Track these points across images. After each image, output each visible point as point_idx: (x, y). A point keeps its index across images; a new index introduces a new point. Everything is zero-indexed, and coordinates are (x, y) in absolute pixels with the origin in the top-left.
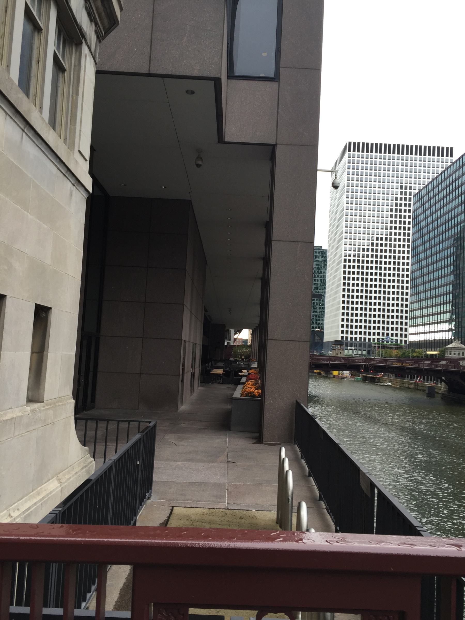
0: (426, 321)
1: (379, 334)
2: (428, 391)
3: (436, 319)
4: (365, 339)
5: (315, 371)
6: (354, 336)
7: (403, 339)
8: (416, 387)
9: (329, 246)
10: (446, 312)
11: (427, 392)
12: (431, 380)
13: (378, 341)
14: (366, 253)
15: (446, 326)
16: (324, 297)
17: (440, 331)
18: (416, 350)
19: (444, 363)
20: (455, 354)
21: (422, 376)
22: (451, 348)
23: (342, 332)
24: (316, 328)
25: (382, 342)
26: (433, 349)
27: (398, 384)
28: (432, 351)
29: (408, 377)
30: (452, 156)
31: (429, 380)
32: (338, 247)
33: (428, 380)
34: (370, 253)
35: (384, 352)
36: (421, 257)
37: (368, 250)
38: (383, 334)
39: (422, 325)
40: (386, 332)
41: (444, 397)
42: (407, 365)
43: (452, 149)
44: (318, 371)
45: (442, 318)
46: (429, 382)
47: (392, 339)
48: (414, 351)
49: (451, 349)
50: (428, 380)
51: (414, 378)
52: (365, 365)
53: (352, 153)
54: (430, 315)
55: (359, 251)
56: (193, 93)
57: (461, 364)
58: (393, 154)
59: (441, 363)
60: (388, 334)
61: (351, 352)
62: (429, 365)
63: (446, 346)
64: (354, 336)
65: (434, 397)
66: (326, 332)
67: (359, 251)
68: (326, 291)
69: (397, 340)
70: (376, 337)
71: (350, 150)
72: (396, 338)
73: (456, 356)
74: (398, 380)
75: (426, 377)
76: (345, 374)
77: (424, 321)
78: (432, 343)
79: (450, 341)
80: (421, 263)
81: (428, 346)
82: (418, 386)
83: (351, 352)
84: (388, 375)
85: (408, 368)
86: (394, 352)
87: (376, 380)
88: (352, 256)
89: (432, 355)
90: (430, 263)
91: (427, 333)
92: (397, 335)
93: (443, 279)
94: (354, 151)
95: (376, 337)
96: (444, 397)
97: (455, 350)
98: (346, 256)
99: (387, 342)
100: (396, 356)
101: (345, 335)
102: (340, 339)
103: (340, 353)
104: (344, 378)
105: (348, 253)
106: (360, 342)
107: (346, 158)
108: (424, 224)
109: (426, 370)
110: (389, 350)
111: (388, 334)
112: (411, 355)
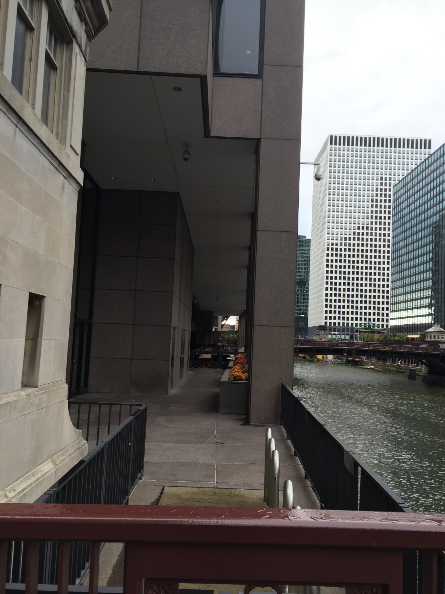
5: (300, 355)
7: (385, 323)
8: (398, 369)
9: (312, 236)
12: (412, 363)
13: (360, 326)
15: (426, 311)
16: (308, 284)
18: (397, 334)
19: (424, 346)
20: (434, 338)
21: (403, 360)
22: (431, 332)
23: (326, 318)
24: (300, 314)
26: (414, 333)
27: (380, 367)
28: (412, 335)
29: (390, 360)
30: (430, 148)
31: (410, 362)
33: (409, 362)
35: (366, 336)
41: (425, 379)
42: (389, 348)
43: (430, 141)
44: (303, 355)
46: (410, 364)
48: (395, 335)
50: (409, 362)
51: (396, 361)
52: (348, 349)
53: (333, 146)
54: (410, 301)
57: (441, 347)
59: (422, 346)
61: (334, 337)
62: (410, 348)
66: (310, 317)
68: (310, 278)
69: (379, 325)
71: (331, 144)
72: (378, 323)
73: (436, 339)
74: (380, 363)
75: (407, 360)
79: (430, 325)
81: (409, 330)
82: (399, 368)
83: (334, 337)
84: (371, 358)
85: (390, 352)
86: (376, 337)
87: (359, 364)
89: (413, 339)
96: (425, 379)
99: (370, 327)
100: (378, 340)
101: (328, 321)
102: (324, 325)
103: (324, 337)
104: (328, 362)
105: (331, 241)
106: (343, 327)
109: (407, 353)
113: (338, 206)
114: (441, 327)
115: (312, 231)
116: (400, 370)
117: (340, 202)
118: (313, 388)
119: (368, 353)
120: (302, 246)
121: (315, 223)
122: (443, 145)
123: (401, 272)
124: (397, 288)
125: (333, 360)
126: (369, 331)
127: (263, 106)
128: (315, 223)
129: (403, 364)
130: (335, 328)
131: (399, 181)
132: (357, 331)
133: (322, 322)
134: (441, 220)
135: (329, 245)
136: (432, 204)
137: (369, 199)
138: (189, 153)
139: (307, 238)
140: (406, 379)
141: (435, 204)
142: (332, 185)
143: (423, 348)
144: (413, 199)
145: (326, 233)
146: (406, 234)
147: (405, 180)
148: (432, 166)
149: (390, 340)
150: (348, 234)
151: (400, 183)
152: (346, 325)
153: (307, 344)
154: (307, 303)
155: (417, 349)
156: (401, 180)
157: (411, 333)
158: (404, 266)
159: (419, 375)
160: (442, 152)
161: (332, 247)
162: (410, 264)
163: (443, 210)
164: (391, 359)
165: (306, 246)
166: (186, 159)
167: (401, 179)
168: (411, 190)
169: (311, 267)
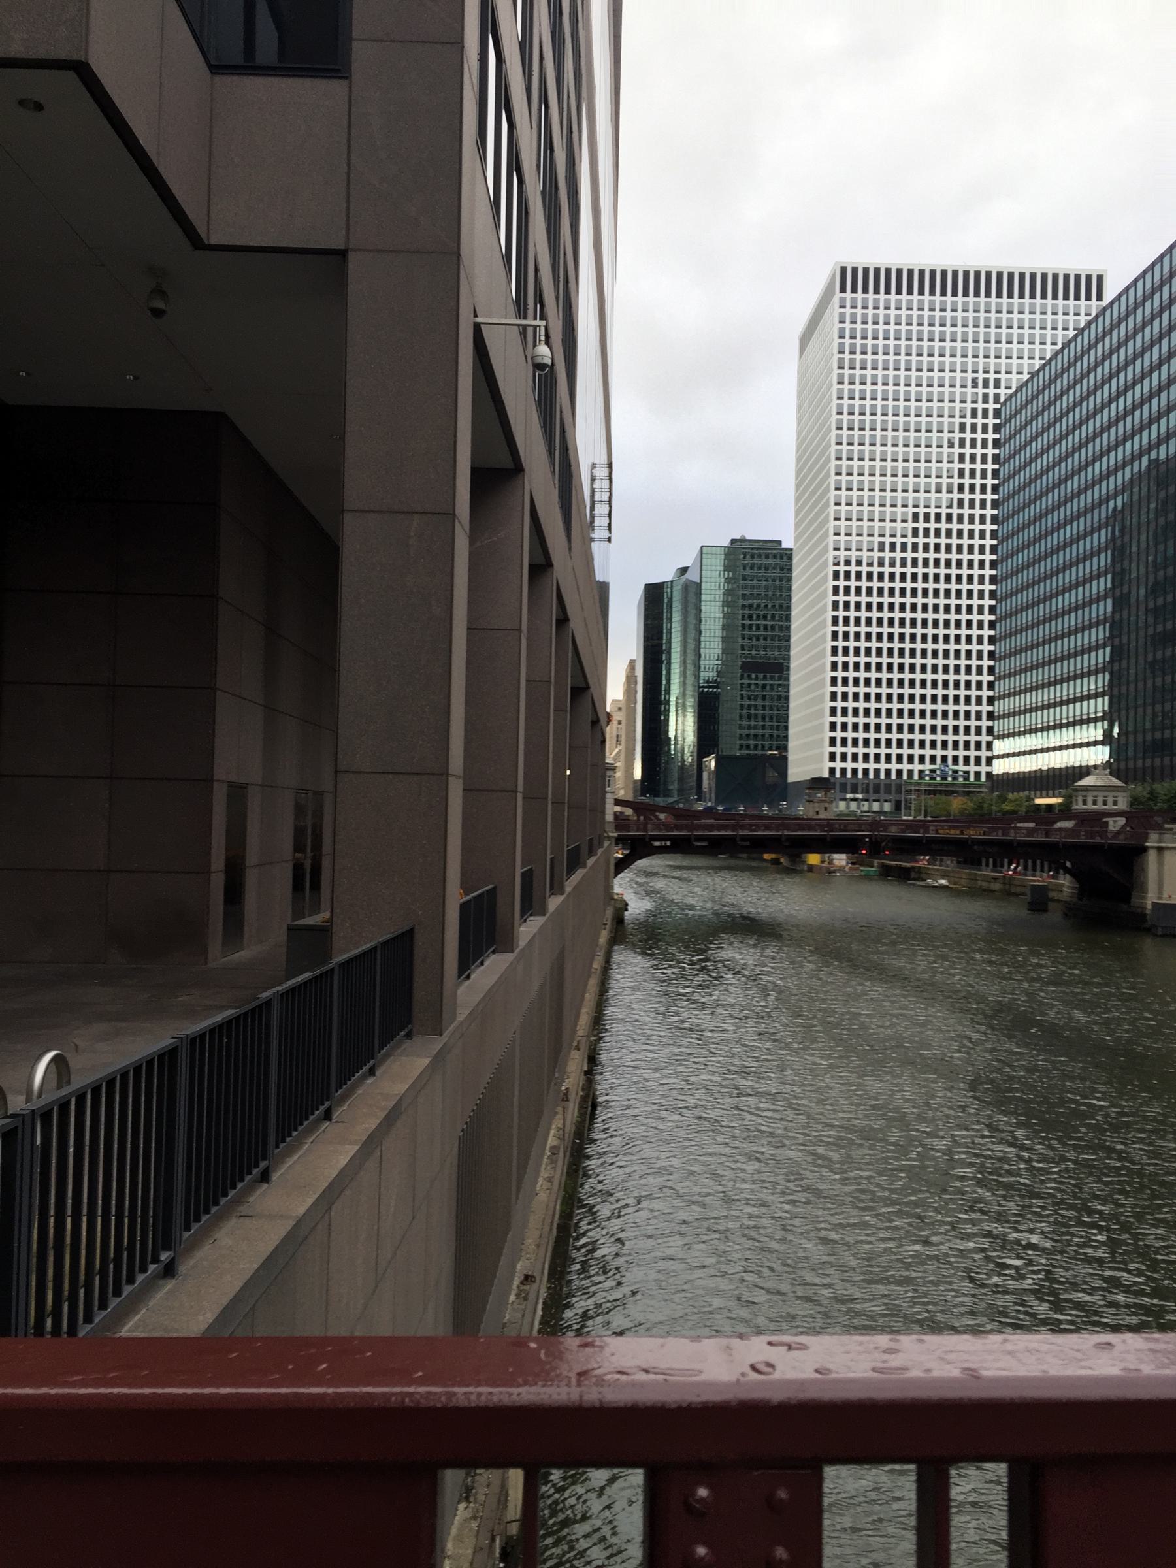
1: (922, 759)
5: (767, 856)
7: (984, 769)
8: (1007, 887)
9: (797, 539)
11: (1029, 898)
12: (1042, 871)
13: (921, 778)
14: (898, 555)
15: (1096, 732)
16: (788, 668)
18: (1010, 796)
19: (1068, 824)
20: (1095, 803)
21: (1021, 861)
22: (1087, 789)
23: (832, 757)
27: (963, 882)
28: (1048, 796)
29: (987, 865)
31: (1038, 867)
33: (1034, 869)
34: (909, 555)
35: (931, 803)
37: (904, 547)
40: (939, 752)
41: (1070, 911)
43: (1100, 279)
44: (773, 856)
46: (1038, 873)
47: (956, 772)
48: (1003, 799)
49: (1087, 790)
50: (1034, 869)
51: (1002, 866)
53: (848, 295)
55: (881, 549)
56: (39, 107)
57: (1111, 828)
59: (1059, 825)
62: (1030, 831)
64: (861, 766)
65: (1046, 911)
66: (792, 756)
67: (881, 549)
69: (967, 773)
71: (843, 290)
72: (966, 768)
73: (1100, 807)
74: (966, 871)
75: (1038, 862)
76: (837, 863)
80: (1061, 575)
84: (941, 861)
87: (913, 875)
89: (1049, 806)
92: (967, 760)
95: (916, 767)
96: (1070, 911)
97: (1095, 793)
99: (944, 778)
101: (838, 765)
102: (826, 775)
103: (826, 809)
104: (834, 871)
105: (843, 554)
106: (877, 781)
107: (834, 310)
110: (944, 798)
112: (994, 808)
113: (861, 459)
114: (1111, 774)
115: (797, 526)
116: (1013, 890)
117: (867, 448)
119: (937, 848)
122: (1171, 248)
123: (1038, 625)
124: (1032, 668)
125: (847, 869)
126: (940, 789)
129: (1020, 874)
130: (890, 785)
131: (1033, 375)
132: (909, 792)
133: (821, 770)
134: (1136, 483)
136: (1121, 432)
139: (784, 546)
140: (1024, 913)
141: (1121, 438)
142: (846, 402)
143: (1061, 829)
144: (1058, 432)
145: (832, 532)
146: (1032, 532)
147: (1093, 326)
150: (887, 534)
151: (1035, 379)
152: (882, 776)
153: (767, 828)
154: (786, 719)
155: (1047, 835)
156: (1039, 371)
157: (1044, 793)
158: (1027, 617)
160: (1166, 269)
161: (848, 568)
162: (1041, 611)
163: (1168, 437)
164: (991, 860)
165: (782, 569)
167: (1037, 368)
168: (1058, 403)
169: (794, 625)
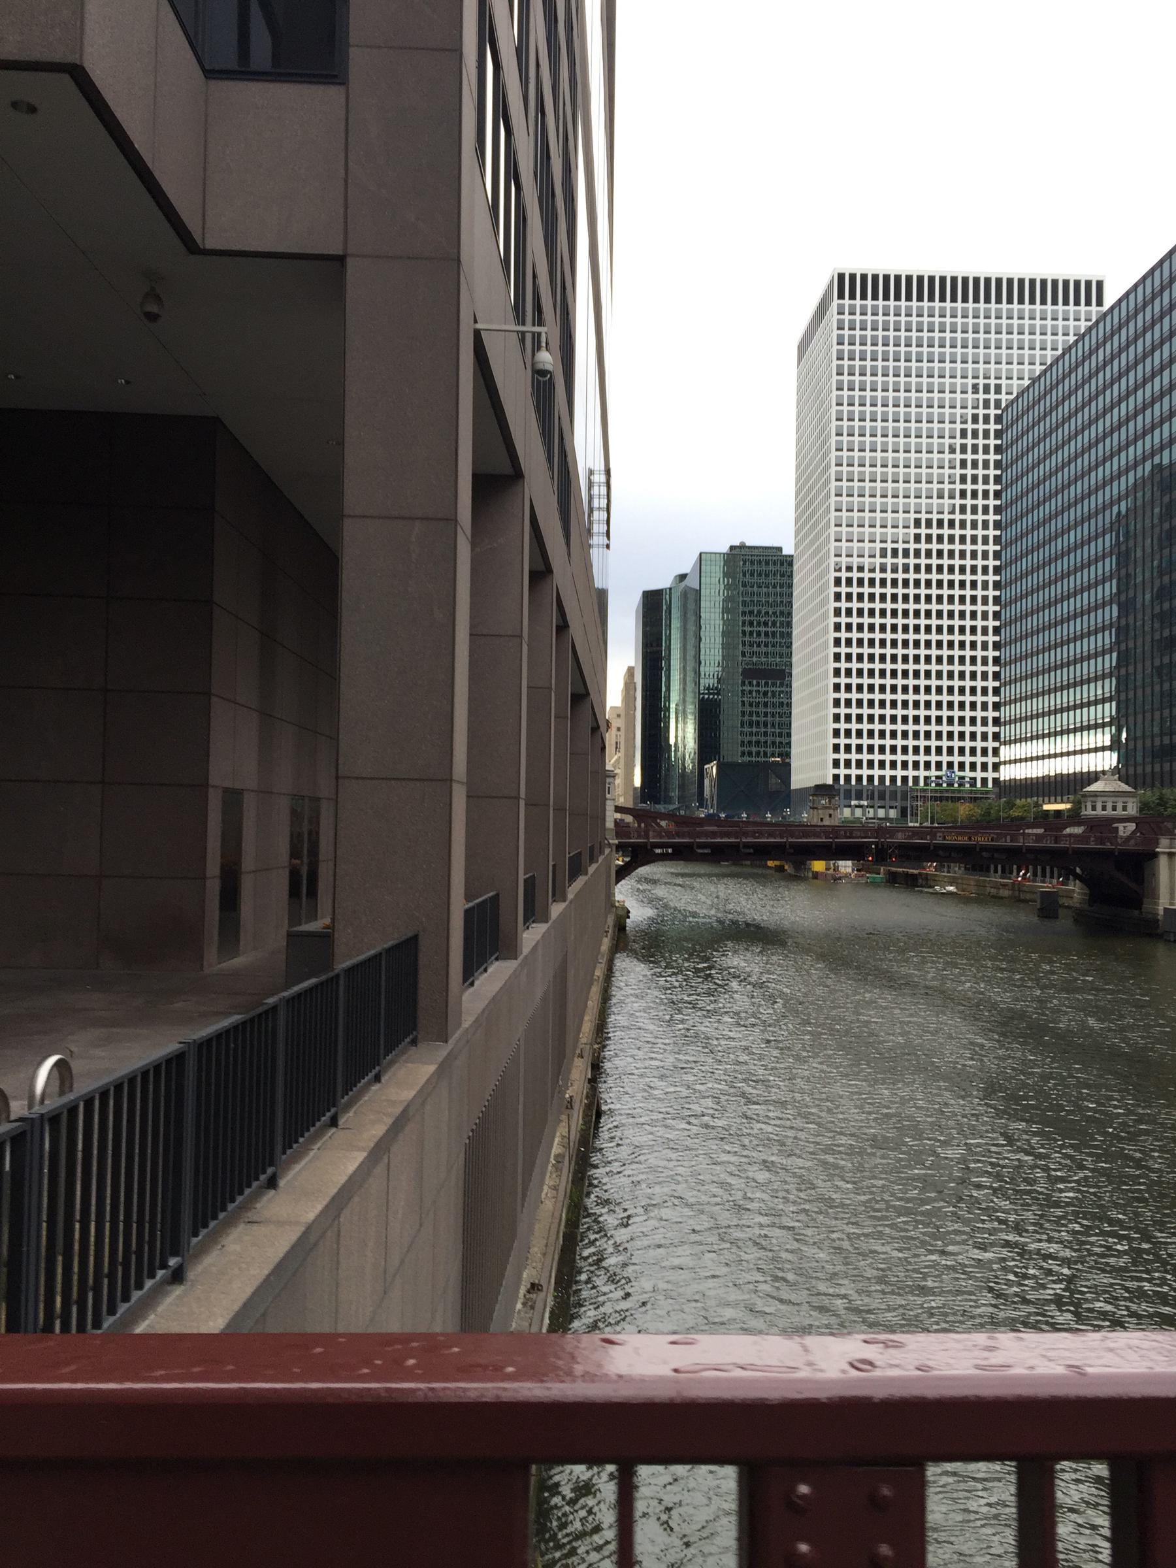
0: (1040, 728)
2: (1042, 903)
3: (1065, 723)
4: (893, 779)
5: (770, 863)
6: (865, 772)
9: (797, 546)
10: (1103, 701)
11: (1038, 905)
13: (926, 784)
15: (1104, 738)
16: (790, 675)
17: (1075, 753)
19: (1078, 830)
20: (1104, 808)
22: (1095, 794)
23: (836, 764)
24: (773, 755)
25: (937, 785)
26: (1059, 798)
27: (973, 889)
28: (1056, 802)
29: (996, 871)
30: (1100, 303)
31: (1048, 874)
32: (818, 550)
33: (1044, 875)
35: (938, 809)
36: (1024, 567)
38: (939, 765)
39: (1032, 738)
41: (1080, 917)
42: (982, 840)
43: (1100, 284)
45: (1078, 719)
46: (1048, 879)
49: (1096, 796)
50: (1044, 875)
51: (1011, 873)
52: (876, 844)
53: (847, 302)
54: (1056, 712)
57: (1121, 833)
58: (896, 299)
59: (1068, 831)
60: (950, 765)
61: (858, 813)
62: (1039, 838)
63: (1083, 788)
66: (795, 763)
68: (794, 659)
69: (974, 779)
70: (922, 773)
71: (841, 296)
72: (973, 774)
73: (1109, 812)
74: (973, 879)
75: (1039, 868)
76: (842, 870)
77: (1035, 729)
78: (1069, 781)
79: (1093, 776)
81: (1047, 791)
82: (1019, 891)
83: (858, 813)
84: (949, 867)
85: (984, 848)
86: (963, 810)
88: (855, 569)
90: (1053, 578)
91: (1043, 757)
93: (1079, 620)
94: (852, 296)
96: (1080, 917)
97: (1105, 799)
98: (840, 570)
99: (950, 784)
100: (969, 817)
101: (842, 772)
102: (830, 781)
104: (840, 878)
105: (844, 561)
106: (882, 788)
108: (1036, 477)
109: (1030, 850)
110: (950, 804)
111: (950, 765)
114: (1120, 779)
116: (1022, 897)
118: (806, 951)
119: (946, 854)
120: (760, 575)
121: (803, 512)
126: (946, 796)
127: (351, 164)
128: (803, 512)
130: (850, 791)
133: (826, 776)
135: (840, 570)
137: (944, 444)
138: (158, 299)
139: (785, 552)
140: (1035, 919)
143: (1070, 835)
146: (1036, 537)
148: (1101, 351)
149: (998, 819)
158: (1032, 622)
159: (1068, 907)
162: (1046, 616)
166: (152, 317)
